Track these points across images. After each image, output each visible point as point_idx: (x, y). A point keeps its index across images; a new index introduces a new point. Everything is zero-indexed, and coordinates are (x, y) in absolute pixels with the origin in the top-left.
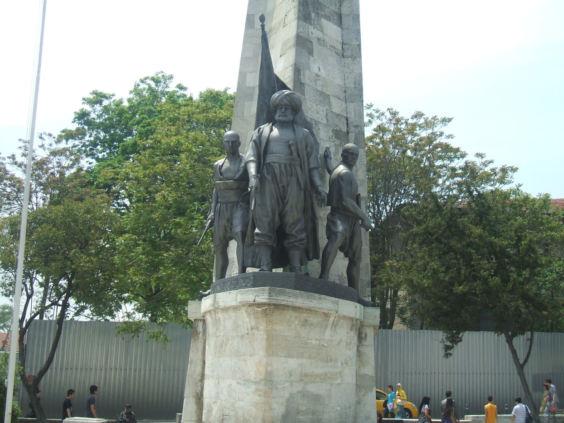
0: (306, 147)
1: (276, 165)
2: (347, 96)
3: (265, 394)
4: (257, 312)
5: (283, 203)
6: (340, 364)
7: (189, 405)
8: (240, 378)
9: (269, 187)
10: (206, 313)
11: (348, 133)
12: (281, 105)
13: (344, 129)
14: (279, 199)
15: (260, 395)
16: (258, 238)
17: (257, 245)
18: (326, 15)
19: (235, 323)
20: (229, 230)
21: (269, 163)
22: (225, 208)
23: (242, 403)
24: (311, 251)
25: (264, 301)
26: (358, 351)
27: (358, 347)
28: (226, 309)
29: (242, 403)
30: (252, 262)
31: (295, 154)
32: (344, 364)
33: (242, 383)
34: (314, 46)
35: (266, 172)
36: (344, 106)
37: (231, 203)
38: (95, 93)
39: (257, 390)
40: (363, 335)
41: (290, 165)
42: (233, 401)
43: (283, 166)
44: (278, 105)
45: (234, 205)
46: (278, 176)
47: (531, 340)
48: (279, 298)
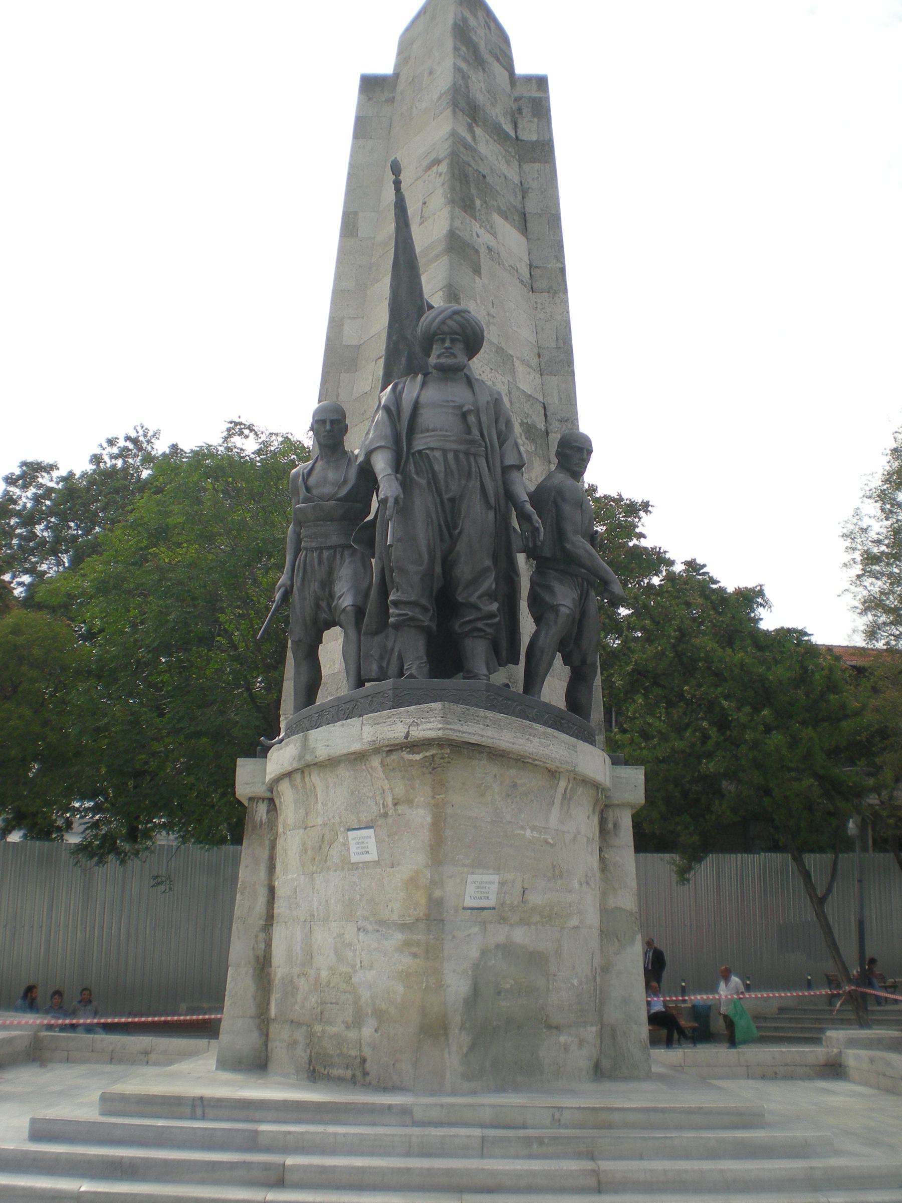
0: (497, 422)
1: (437, 454)
2: (542, 363)
3: (427, 951)
4: (411, 763)
5: (451, 535)
6: (577, 885)
7: (239, 984)
8: (365, 918)
9: (422, 503)
10: (278, 780)
11: (547, 433)
12: (444, 333)
13: (541, 426)
14: (445, 530)
15: (415, 955)
16: (397, 612)
17: (397, 626)
18: (499, 207)
19: (352, 793)
20: (324, 604)
21: (420, 452)
22: (316, 561)
23: (370, 975)
24: (504, 649)
25: (432, 734)
26: (602, 859)
27: (601, 850)
28: (331, 764)
29: (370, 975)
30: (381, 668)
31: (475, 431)
32: (584, 885)
33: (370, 928)
34: (482, 260)
35: (413, 470)
36: (538, 381)
37: (329, 548)
38: (24, 464)
39: (407, 944)
40: (610, 826)
41: (467, 454)
42: (349, 970)
43: (450, 456)
44: (435, 334)
45: (335, 552)
46: (441, 476)
47: (835, 864)
48: (465, 728)
